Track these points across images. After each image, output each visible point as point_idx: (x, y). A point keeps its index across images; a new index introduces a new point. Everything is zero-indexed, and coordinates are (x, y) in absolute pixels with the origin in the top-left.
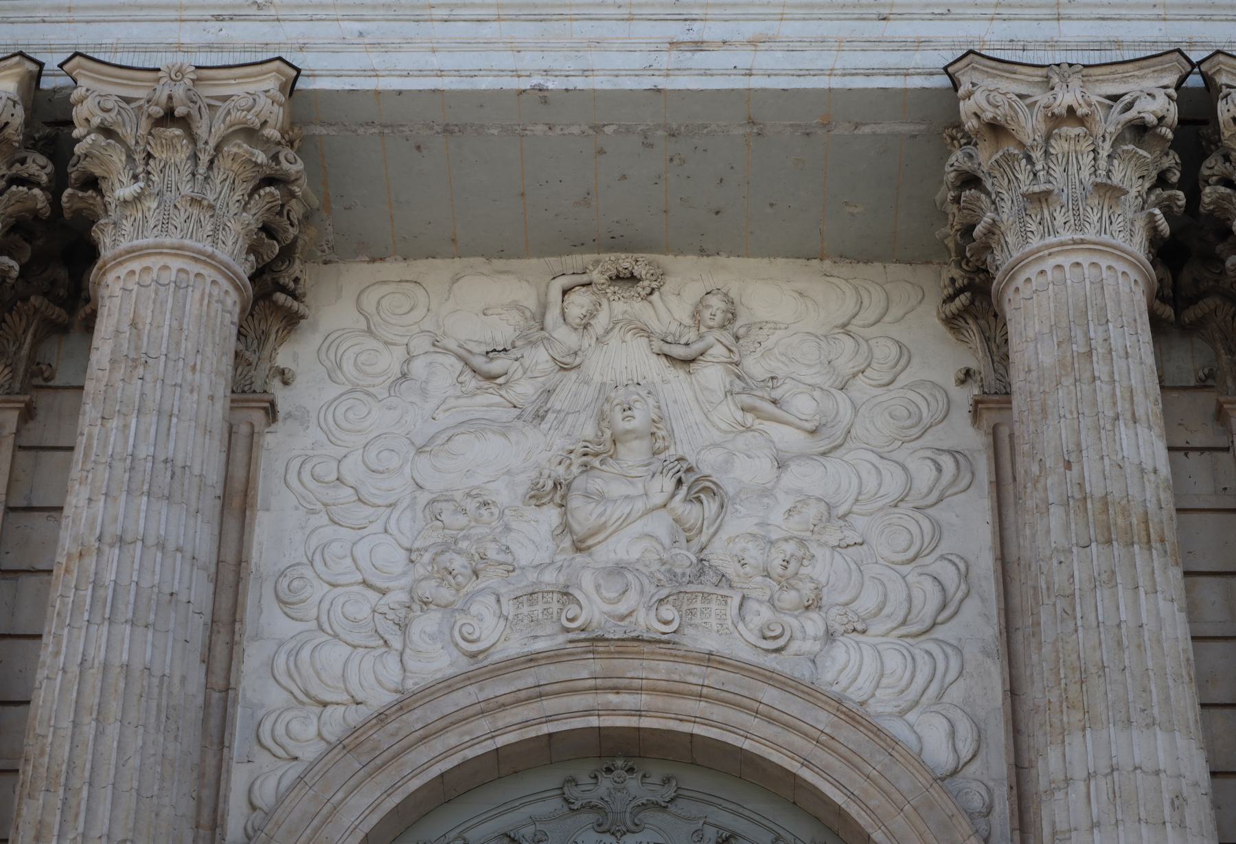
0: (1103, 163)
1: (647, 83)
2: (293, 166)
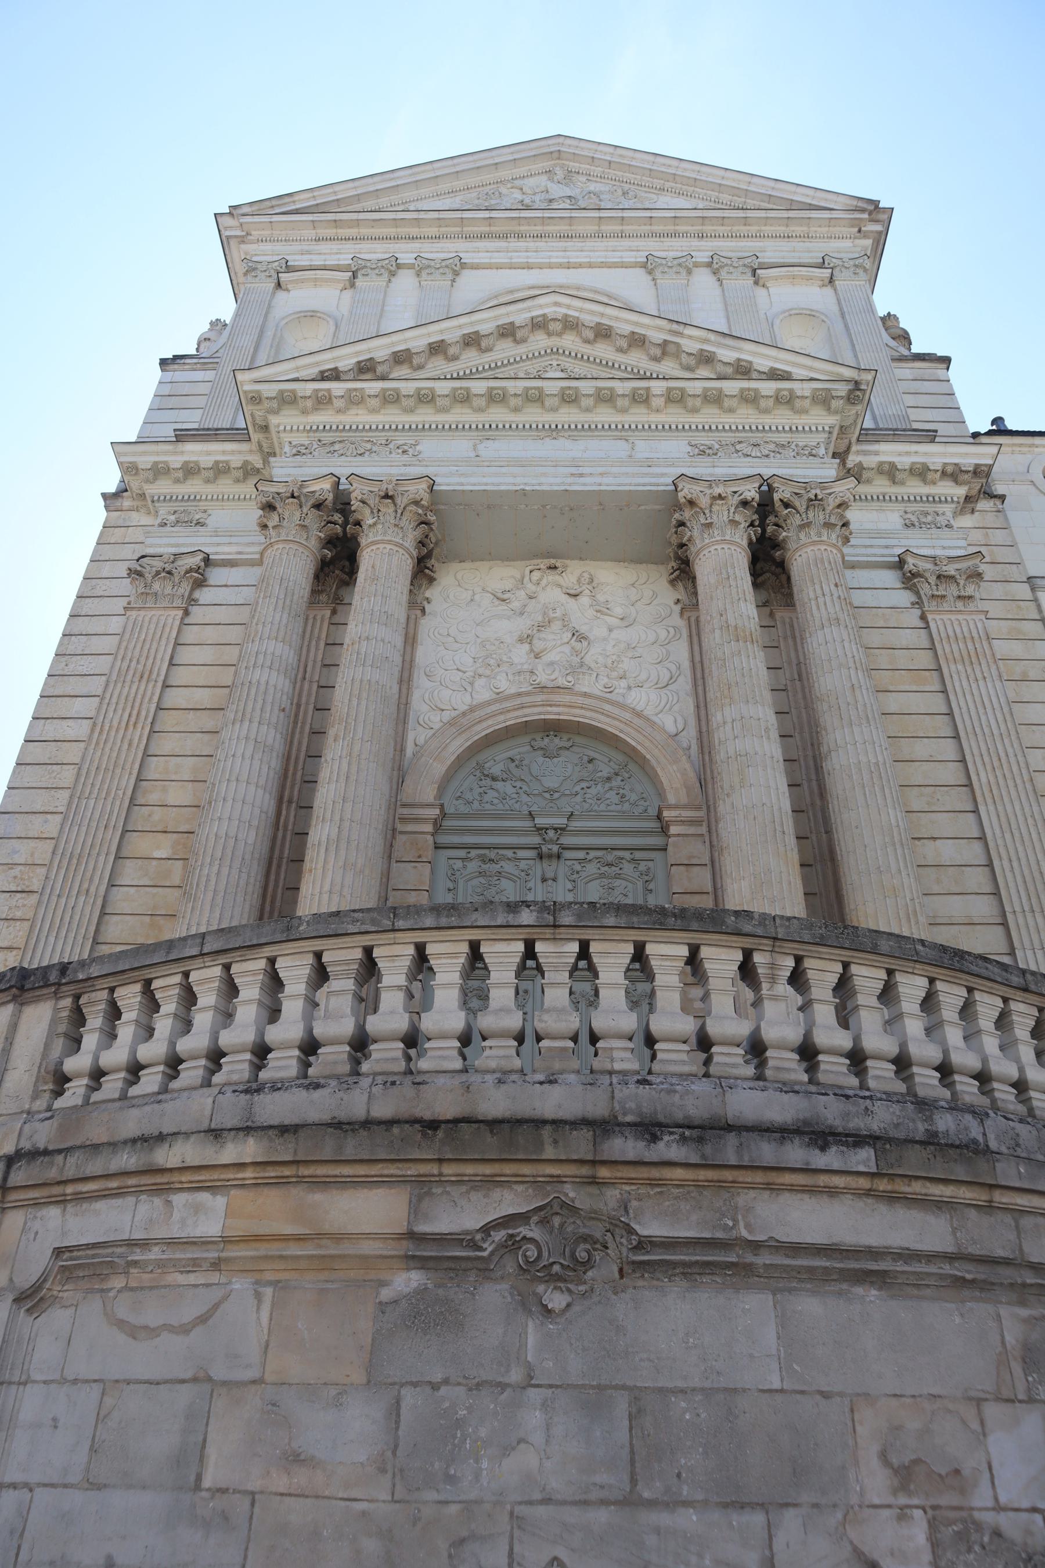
0: (731, 514)
1: (563, 488)
2: (432, 518)
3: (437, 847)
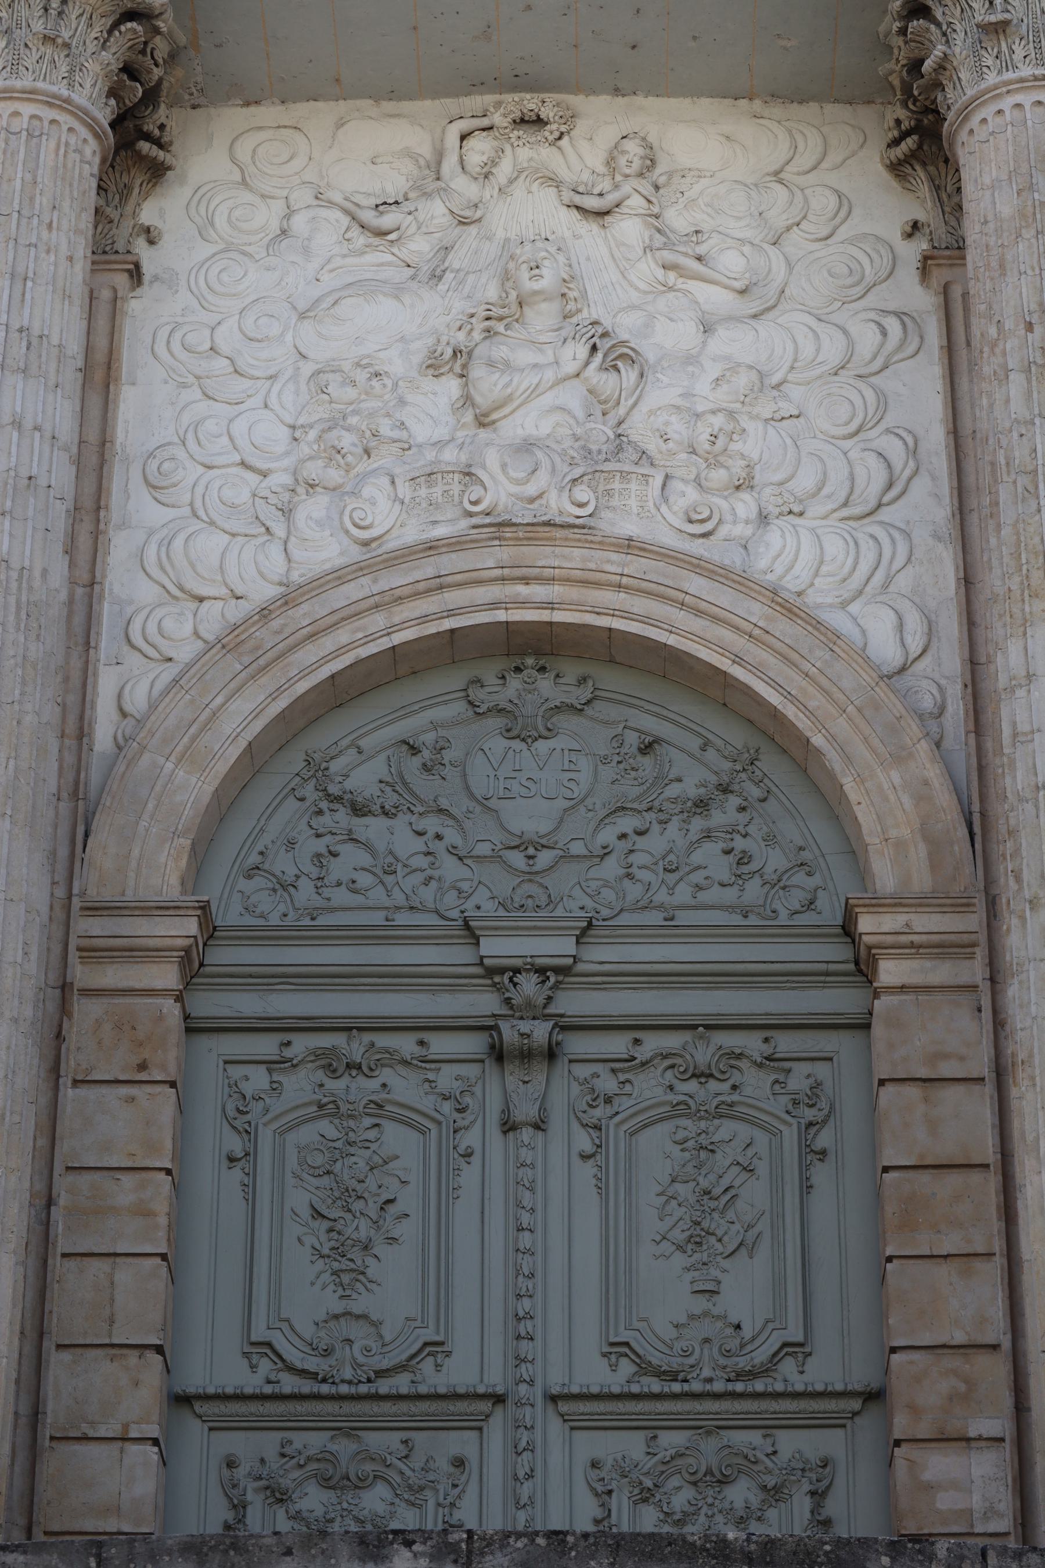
3: (193, 1027)
